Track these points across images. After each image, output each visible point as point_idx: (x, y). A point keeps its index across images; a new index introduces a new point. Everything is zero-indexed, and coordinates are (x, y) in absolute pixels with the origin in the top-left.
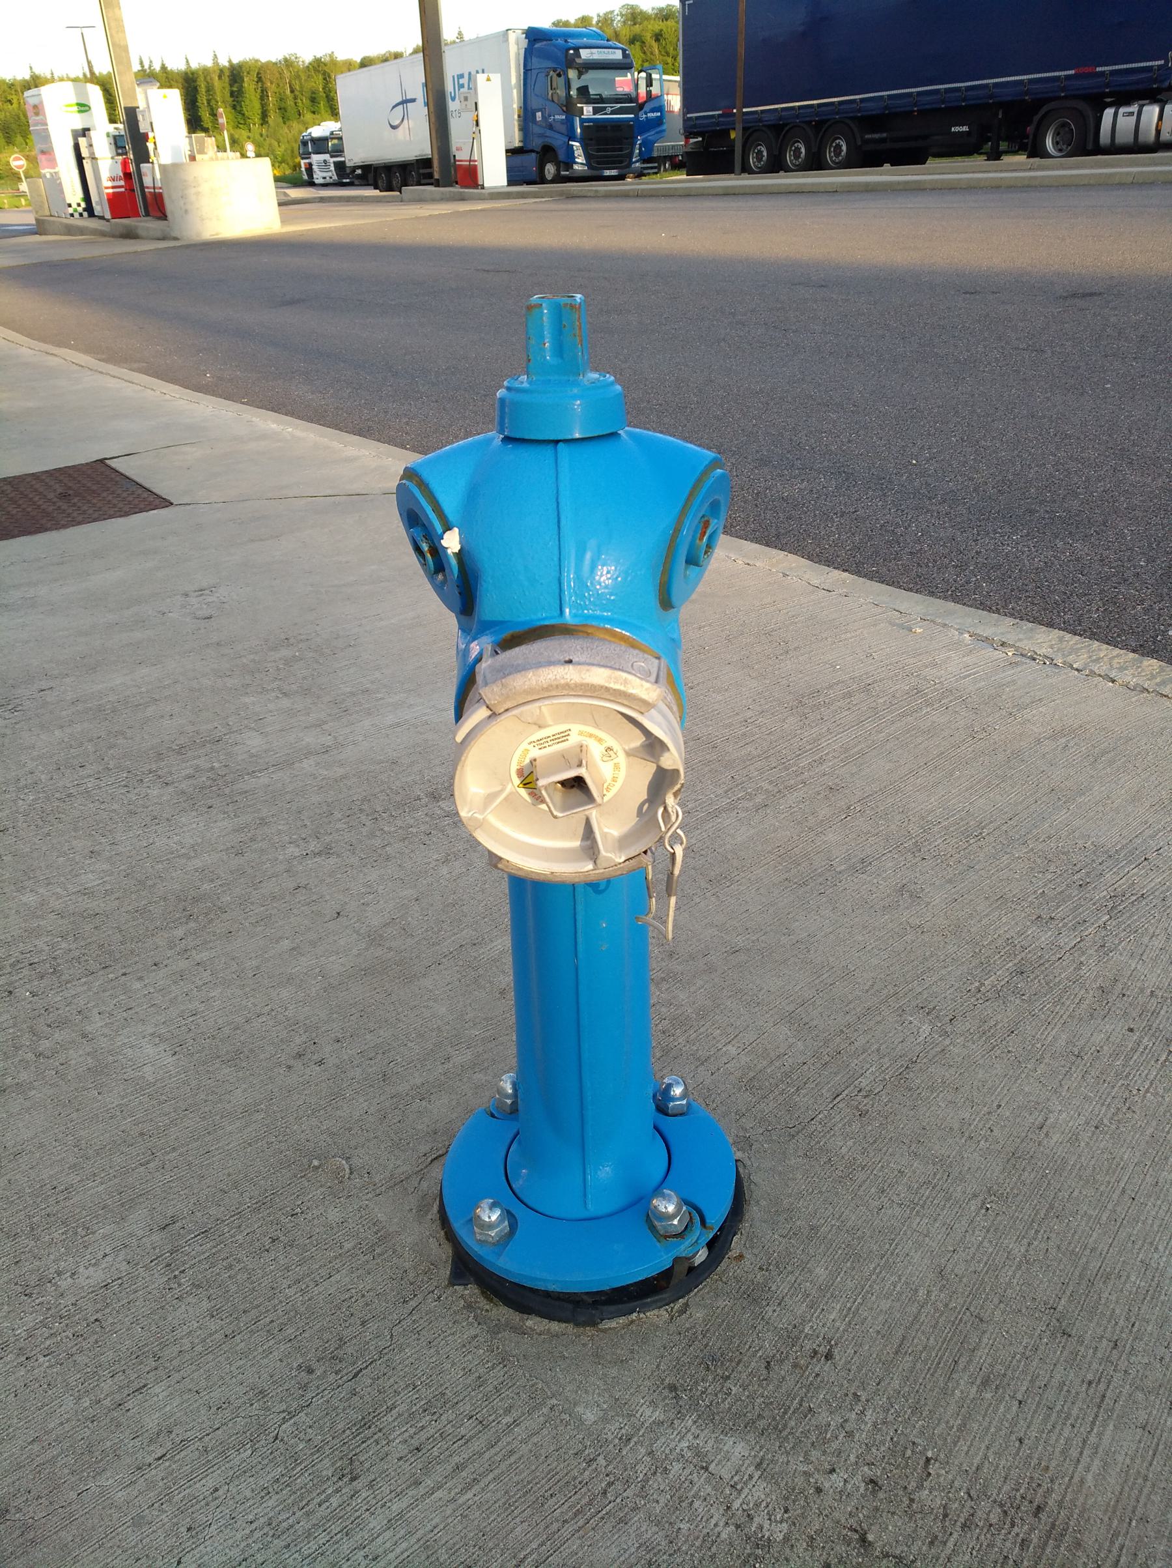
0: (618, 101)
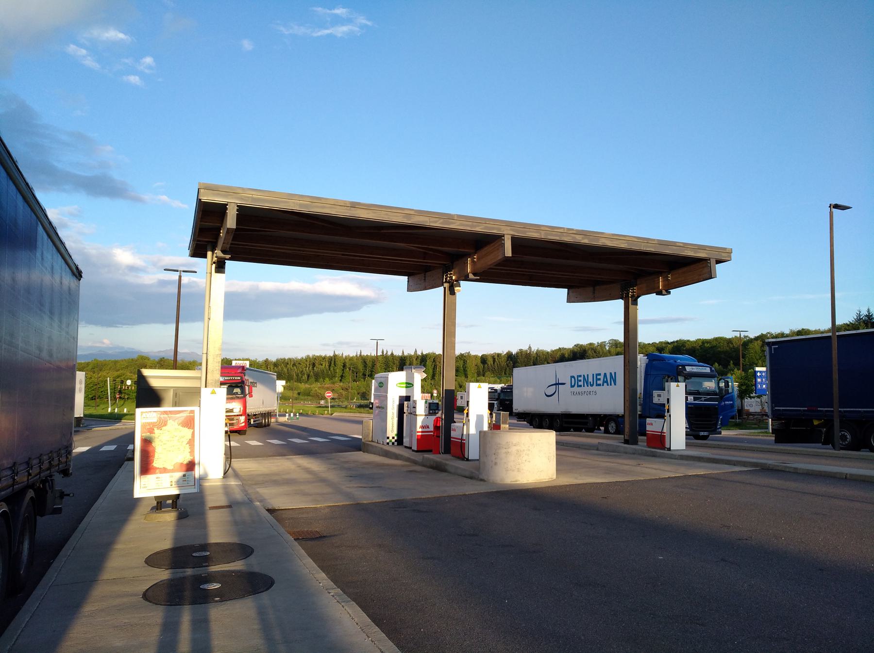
0: (708, 394)
